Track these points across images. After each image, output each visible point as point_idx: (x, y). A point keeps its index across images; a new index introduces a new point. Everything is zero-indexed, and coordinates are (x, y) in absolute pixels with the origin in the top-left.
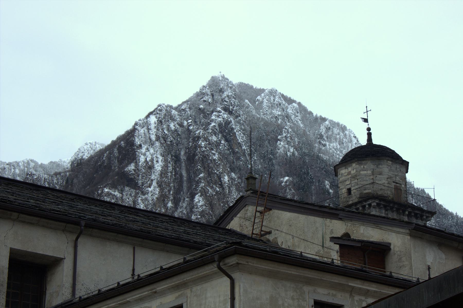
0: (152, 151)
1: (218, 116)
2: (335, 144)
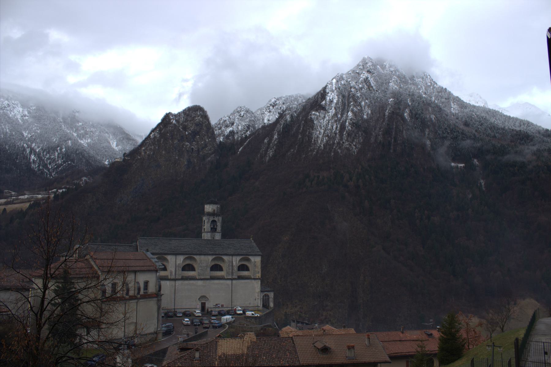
0: (333, 94)
1: (364, 75)
2: (419, 79)
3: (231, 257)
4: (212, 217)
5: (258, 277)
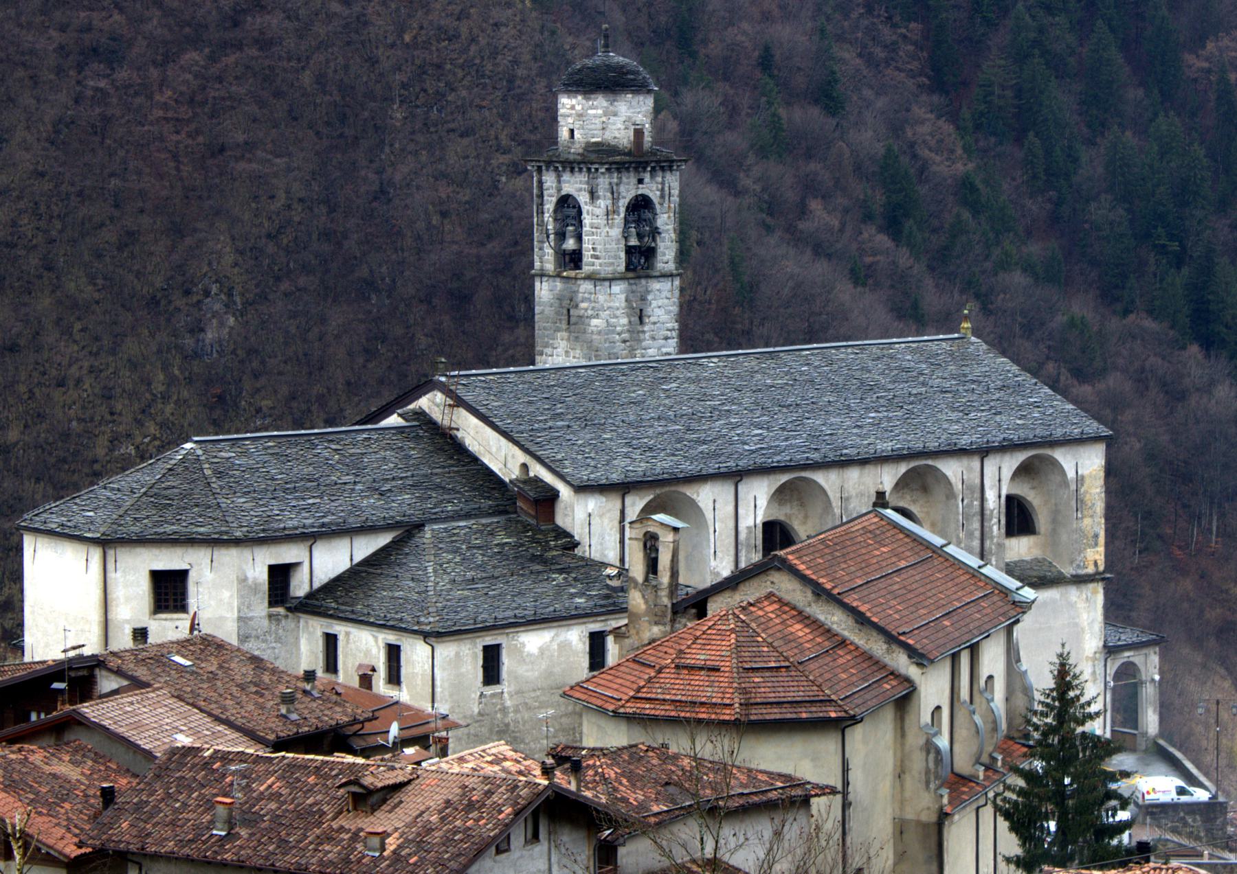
3: (976, 463)
4: (634, 180)
5: (1091, 570)
